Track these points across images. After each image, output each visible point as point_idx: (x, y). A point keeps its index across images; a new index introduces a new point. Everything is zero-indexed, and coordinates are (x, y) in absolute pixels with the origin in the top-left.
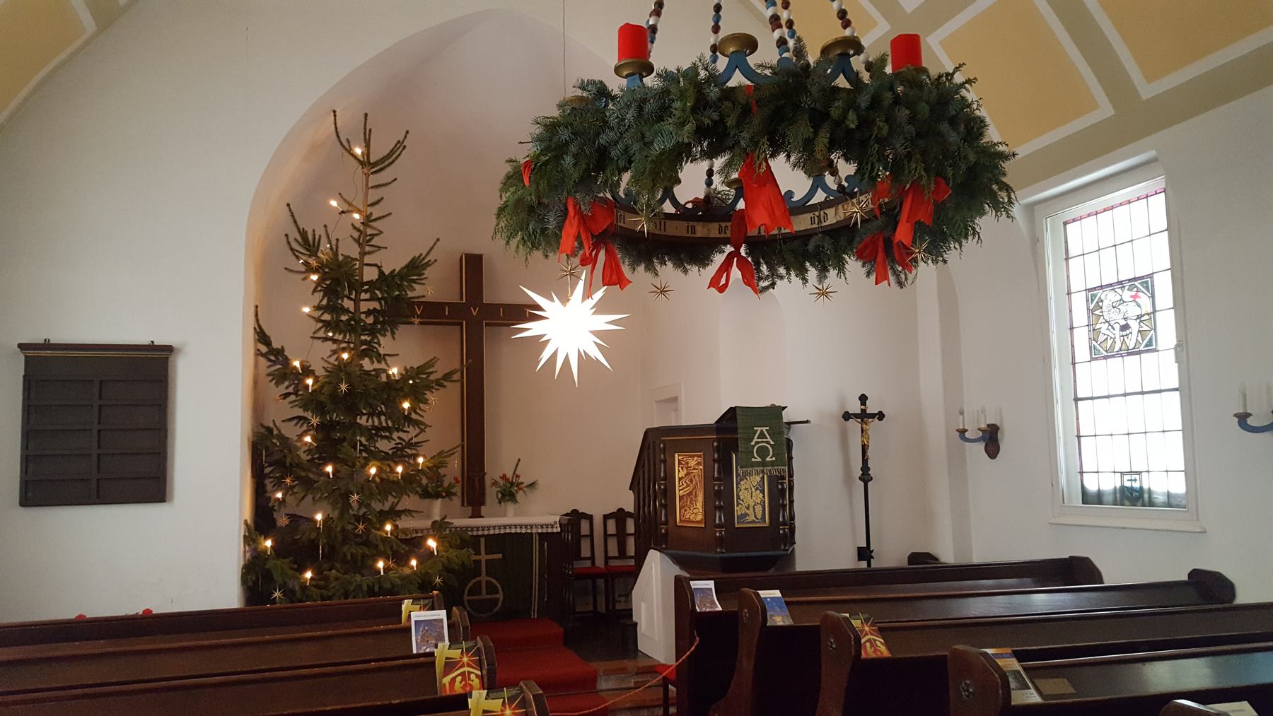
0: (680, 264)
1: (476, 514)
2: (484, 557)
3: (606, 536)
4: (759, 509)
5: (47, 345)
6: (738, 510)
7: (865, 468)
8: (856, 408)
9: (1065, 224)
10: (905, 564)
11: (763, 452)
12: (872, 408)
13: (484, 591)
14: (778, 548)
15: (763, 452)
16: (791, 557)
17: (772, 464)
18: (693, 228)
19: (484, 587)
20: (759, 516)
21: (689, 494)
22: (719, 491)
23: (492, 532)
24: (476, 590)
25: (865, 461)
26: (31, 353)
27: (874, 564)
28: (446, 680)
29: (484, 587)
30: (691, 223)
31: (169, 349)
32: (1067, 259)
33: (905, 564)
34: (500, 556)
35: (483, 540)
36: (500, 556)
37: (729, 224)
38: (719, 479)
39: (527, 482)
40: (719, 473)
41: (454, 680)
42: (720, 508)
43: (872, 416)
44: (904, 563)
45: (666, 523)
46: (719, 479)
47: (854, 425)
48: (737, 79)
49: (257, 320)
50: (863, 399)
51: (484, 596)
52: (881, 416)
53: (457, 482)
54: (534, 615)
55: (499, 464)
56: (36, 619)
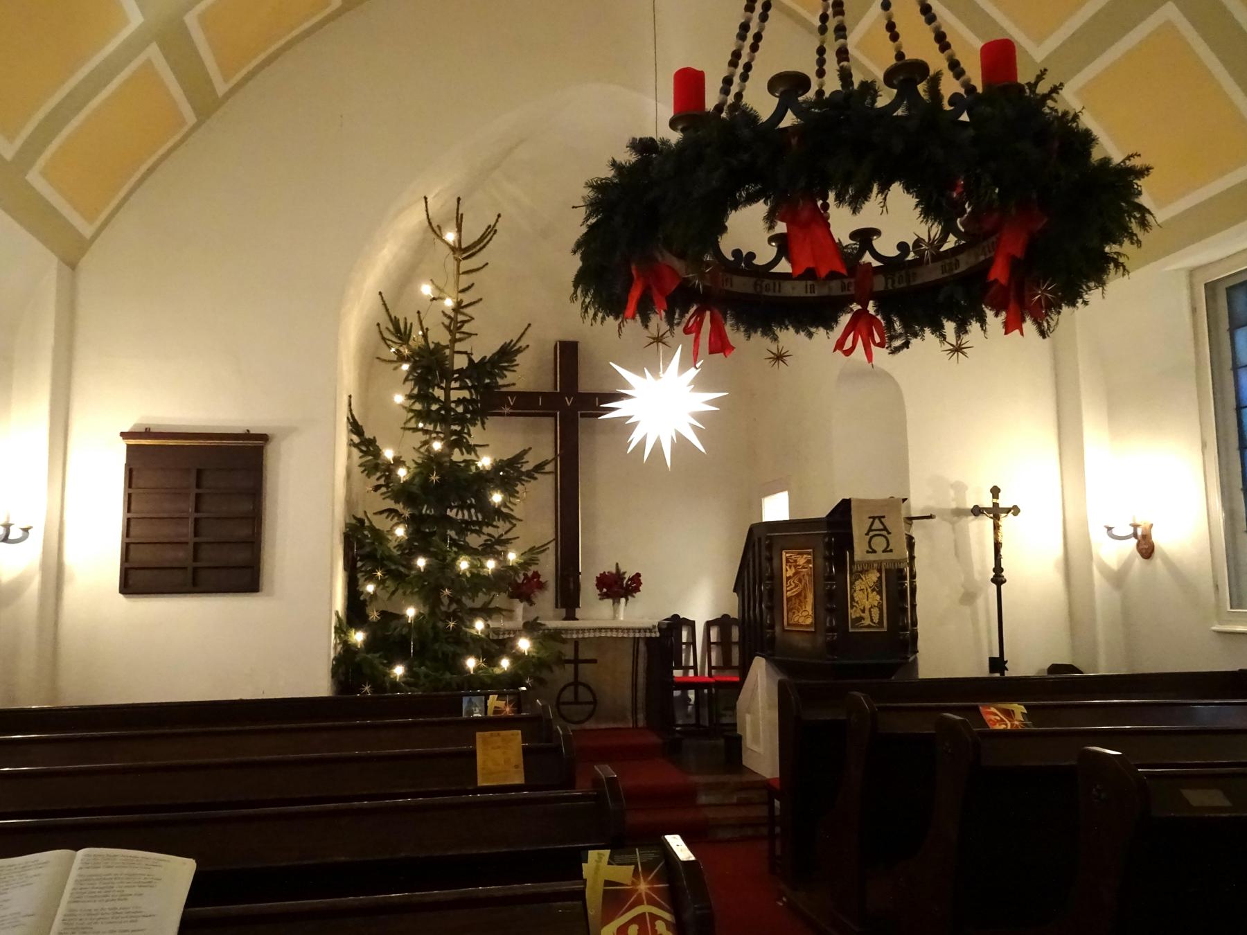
1: (571, 616)
4: (876, 612)
6: (853, 613)
7: (998, 569)
12: (1004, 502)
20: (876, 619)
21: (798, 595)
27: (1007, 674)
28: (993, 709)
31: (264, 438)
43: (1008, 511)
50: (995, 491)
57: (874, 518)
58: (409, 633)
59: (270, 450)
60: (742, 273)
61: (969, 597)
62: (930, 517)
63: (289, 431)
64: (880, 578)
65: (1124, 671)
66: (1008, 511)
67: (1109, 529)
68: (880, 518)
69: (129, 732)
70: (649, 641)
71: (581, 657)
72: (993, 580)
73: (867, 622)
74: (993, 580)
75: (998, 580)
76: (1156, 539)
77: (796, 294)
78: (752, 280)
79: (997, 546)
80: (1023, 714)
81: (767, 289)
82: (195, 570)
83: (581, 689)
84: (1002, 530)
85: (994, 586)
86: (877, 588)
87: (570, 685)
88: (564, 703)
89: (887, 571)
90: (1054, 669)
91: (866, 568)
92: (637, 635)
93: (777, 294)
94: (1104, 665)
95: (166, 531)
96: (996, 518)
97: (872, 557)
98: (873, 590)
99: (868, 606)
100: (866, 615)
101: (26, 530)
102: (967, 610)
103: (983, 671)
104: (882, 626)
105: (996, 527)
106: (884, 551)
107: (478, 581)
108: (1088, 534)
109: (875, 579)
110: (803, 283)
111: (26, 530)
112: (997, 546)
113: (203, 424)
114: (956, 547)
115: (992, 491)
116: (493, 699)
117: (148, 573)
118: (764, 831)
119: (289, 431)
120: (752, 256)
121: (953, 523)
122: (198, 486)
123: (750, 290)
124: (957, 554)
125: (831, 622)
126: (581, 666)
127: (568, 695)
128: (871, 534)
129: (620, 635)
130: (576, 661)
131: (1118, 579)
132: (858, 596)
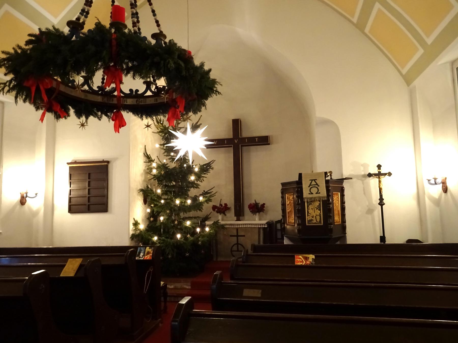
0: (133, 113)
1: (238, 220)
4: (318, 218)
6: (308, 218)
7: (381, 199)
8: (376, 171)
12: (382, 171)
20: (318, 220)
21: (290, 211)
27: (386, 243)
28: (300, 257)
31: (108, 162)
43: (385, 174)
49: (146, 151)
50: (379, 167)
52: (390, 174)
56: (66, 246)
57: (312, 180)
58: (160, 226)
59: (110, 166)
61: (370, 211)
62: (351, 178)
63: (116, 159)
64: (320, 204)
65: (441, 243)
66: (385, 174)
67: (429, 180)
68: (314, 180)
69: (60, 255)
70: (264, 228)
71: (239, 234)
72: (379, 204)
73: (315, 221)
74: (379, 204)
75: (381, 203)
76: (449, 185)
77: (151, 103)
78: (136, 99)
79: (380, 190)
80: (313, 259)
81: (141, 102)
82: (89, 205)
83: (239, 246)
84: (382, 183)
85: (380, 207)
86: (319, 208)
87: (235, 244)
88: (234, 251)
89: (323, 201)
90: (409, 241)
91: (312, 201)
92: (259, 226)
94: (430, 240)
95: (81, 193)
96: (379, 178)
97: (311, 196)
98: (317, 209)
99: (315, 215)
100: (314, 219)
101: (36, 194)
102: (369, 216)
103: (378, 241)
104: (321, 223)
105: (380, 182)
106: (317, 193)
107: (183, 208)
108: (423, 184)
109: (318, 204)
111: (36, 194)
112: (380, 190)
113: (91, 158)
114: (364, 190)
116: (148, 248)
117: (78, 206)
118: (168, 299)
119: (116, 159)
120: (137, 91)
121: (362, 181)
122: (89, 178)
123: (135, 103)
124: (364, 193)
125: (299, 222)
126: (239, 237)
127: (235, 248)
128: (311, 186)
129: (253, 226)
130: (237, 236)
131: (437, 202)
132: (310, 211)
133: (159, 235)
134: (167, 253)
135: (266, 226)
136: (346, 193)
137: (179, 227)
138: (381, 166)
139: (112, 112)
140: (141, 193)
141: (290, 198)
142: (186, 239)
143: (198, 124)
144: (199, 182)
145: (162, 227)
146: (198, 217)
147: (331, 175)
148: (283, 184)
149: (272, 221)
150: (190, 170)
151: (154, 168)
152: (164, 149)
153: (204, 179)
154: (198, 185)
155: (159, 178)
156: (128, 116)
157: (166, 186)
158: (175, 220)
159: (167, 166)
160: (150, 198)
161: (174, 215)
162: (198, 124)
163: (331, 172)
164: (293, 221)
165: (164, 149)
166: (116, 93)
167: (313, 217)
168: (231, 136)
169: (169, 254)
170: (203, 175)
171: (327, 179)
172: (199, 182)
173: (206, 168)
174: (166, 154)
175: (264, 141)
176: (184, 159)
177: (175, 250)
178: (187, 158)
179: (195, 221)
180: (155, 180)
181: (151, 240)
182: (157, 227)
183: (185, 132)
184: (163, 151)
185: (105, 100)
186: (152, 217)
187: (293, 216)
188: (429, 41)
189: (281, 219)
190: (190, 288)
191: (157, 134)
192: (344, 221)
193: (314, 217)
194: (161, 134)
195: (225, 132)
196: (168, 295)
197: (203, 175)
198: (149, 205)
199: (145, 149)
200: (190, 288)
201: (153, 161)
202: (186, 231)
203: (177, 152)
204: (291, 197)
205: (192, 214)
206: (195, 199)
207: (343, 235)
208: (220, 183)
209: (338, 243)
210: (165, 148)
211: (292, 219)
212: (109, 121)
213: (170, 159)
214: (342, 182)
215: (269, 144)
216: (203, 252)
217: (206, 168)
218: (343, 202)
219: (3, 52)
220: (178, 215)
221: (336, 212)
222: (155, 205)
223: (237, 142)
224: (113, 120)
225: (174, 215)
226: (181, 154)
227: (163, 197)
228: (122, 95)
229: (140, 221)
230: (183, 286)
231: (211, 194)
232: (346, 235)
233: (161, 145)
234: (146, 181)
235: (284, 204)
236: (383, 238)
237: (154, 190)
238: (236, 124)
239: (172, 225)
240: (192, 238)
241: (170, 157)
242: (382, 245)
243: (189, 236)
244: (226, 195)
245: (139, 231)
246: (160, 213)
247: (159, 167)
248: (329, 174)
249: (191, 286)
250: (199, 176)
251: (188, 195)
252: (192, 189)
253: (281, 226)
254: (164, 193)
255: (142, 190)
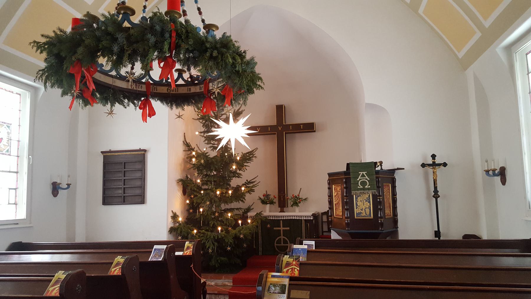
1: (282, 211)
2: (282, 228)
3: (322, 222)
4: (367, 210)
5: (110, 152)
6: (356, 211)
7: (436, 191)
8: (430, 161)
9: (527, 54)
10: (461, 238)
11: (363, 184)
12: (438, 161)
13: (282, 242)
14: (378, 229)
15: (363, 184)
16: (395, 232)
17: (368, 189)
18: (190, 89)
19: (282, 240)
20: (368, 214)
21: (338, 203)
22: (346, 202)
23: (285, 218)
24: (279, 242)
25: (436, 188)
26: (105, 154)
27: (441, 238)
28: (113, 270)
29: (282, 240)
30: (189, 87)
31: (145, 151)
32: (528, 74)
33: (461, 238)
34: (289, 228)
35: (281, 221)
36: (289, 228)
37: (203, 86)
38: (346, 196)
39: (304, 198)
40: (346, 193)
41: (116, 270)
42: (347, 209)
43: (439, 165)
44: (461, 238)
45: (331, 216)
46: (346, 196)
47: (430, 170)
48: (126, 24)
49: (185, 138)
50: (433, 156)
51: (282, 244)
52: (445, 165)
53: (275, 198)
54: (260, 253)
55: (292, 191)
60: (164, 85)
72: (434, 196)
73: (364, 214)
74: (434, 196)
90: (466, 236)
93: (177, 92)
99: (364, 208)
103: (429, 236)
107: (224, 198)
110: (187, 88)
115: (432, 156)
133: (199, 229)
134: (207, 247)
135: (312, 218)
136: (397, 184)
137: (220, 219)
138: (436, 156)
139: (139, 99)
140: (180, 183)
141: (337, 190)
142: (227, 232)
143: (240, 111)
144: (241, 172)
145: (202, 219)
146: (240, 208)
147: (381, 166)
148: (330, 175)
149: (318, 213)
150: (231, 159)
151: (194, 156)
152: (205, 137)
153: (247, 168)
154: (240, 174)
155: (198, 167)
156: (156, 104)
157: (206, 175)
158: (216, 212)
159: (207, 155)
160: (189, 188)
161: (214, 206)
162: (240, 111)
163: (381, 163)
164: (341, 214)
165: (205, 137)
166: (144, 81)
167: (362, 210)
168: (274, 123)
169: (209, 247)
170: (245, 164)
171: (377, 169)
172: (241, 172)
173: (248, 156)
174: (206, 142)
175: (309, 128)
176: (226, 148)
177: (216, 244)
178: (229, 146)
179: (236, 212)
180: (195, 169)
181: (190, 233)
182: (197, 219)
183: (227, 121)
184: (204, 139)
185: (134, 87)
186: (192, 207)
187: (341, 208)
188: (487, 24)
189: (328, 211)
190: (232, 285)
191: (197, 121)
192: (395, 214)
193: (364, 210)
194: (201, 121)
195: (267, 118)
196: (208, 292)
197: (245, 164)
198: (189, 196)
199: (185, 136)
200: (232, 285)
201: (193, 150)
202: (228, 224)
203: (220, 140)
204: (339, 188)
205: (234, 205)
206: (237, 189)
207: (394, 229)
208: (260, 174)
209: (388, 239)
210: (205, 135)
211: (338, 212)
212: (136, 109)
213: (210, 147)
214: (394, 173)
215: (315, 131)
216: (245, 245)
217: (248, 157)
218: (394, 194)
219: (42, 36)
220: (219, 206)
221: (387, 205)
222: (195, 196)
223: (282, 130)
224: (140, 108)
225: (214, 206)
226: (223, 143)
227: (204, 187)
228: (151, 82)
229: (178, 213)
230: (224, 283)
231: (254, 184)
232: (398, 229)
233: (201, 132)
234: (185, 170)
235: (330, 196)
236: (437, 233)
237: (194, 180)
238: (280, 109)
239: (213, 217)
240: (234, 232)
241: (211, 145)
242: (436, 241)
243: (230, 228)
244: (267, 184)
245: (178, 224)
246: (199, 204)
247: (198, 156)
248: (379, 164)
249: (233, 282)
250: (241, 165)
251: (230, 185)
252: (234, 178)
253: (328, 218)
254: (204, 183)
255: (181, 180)
